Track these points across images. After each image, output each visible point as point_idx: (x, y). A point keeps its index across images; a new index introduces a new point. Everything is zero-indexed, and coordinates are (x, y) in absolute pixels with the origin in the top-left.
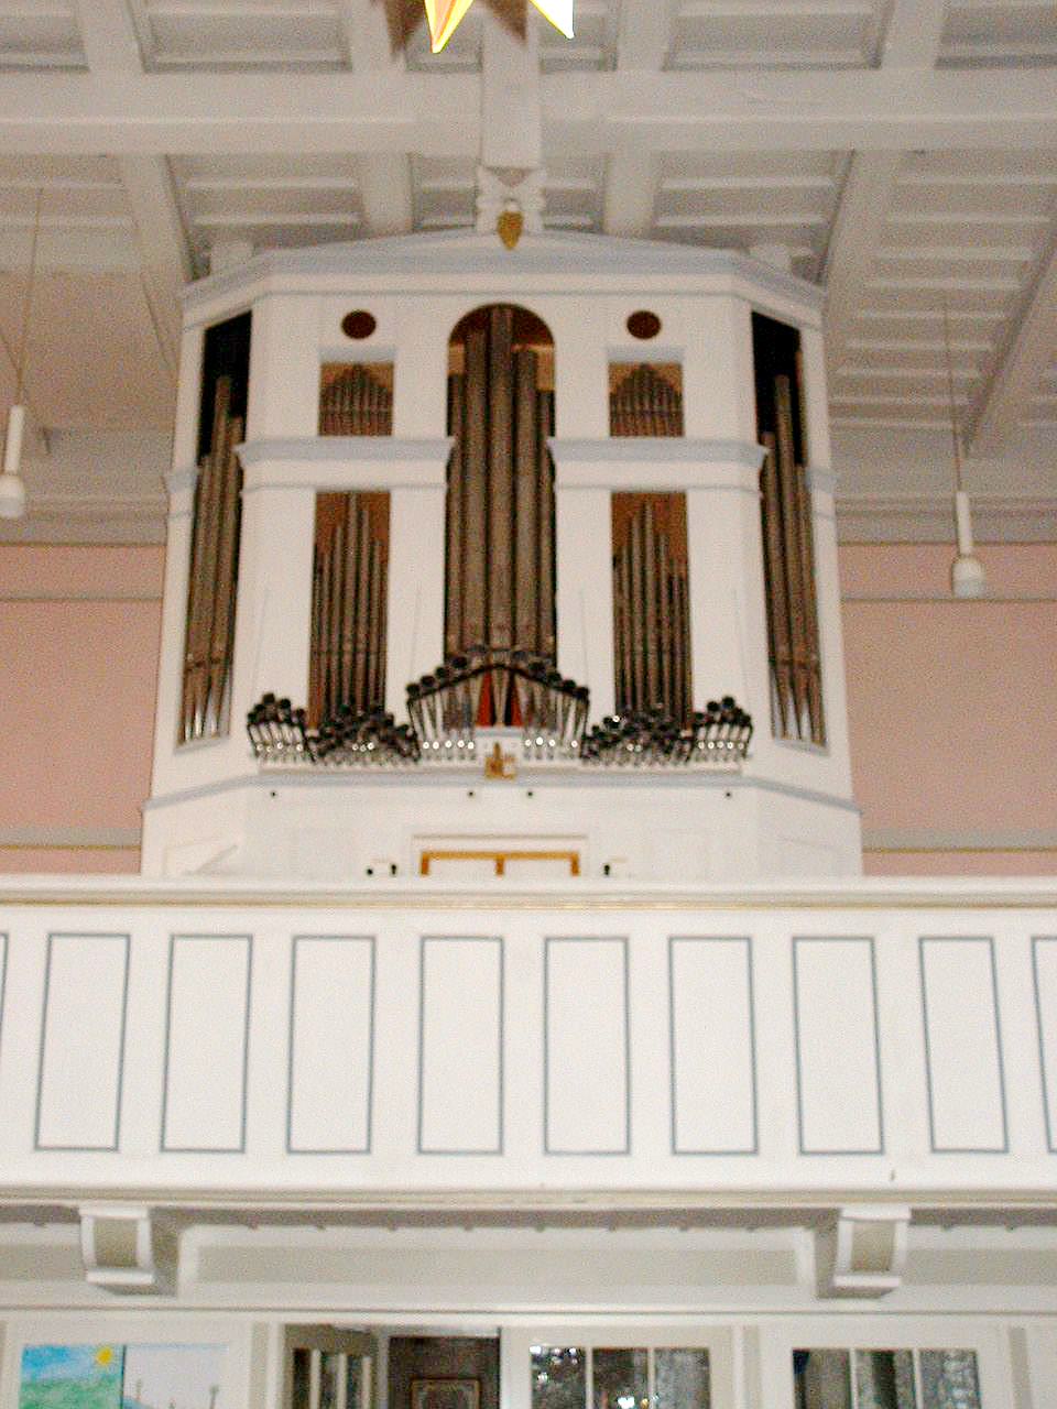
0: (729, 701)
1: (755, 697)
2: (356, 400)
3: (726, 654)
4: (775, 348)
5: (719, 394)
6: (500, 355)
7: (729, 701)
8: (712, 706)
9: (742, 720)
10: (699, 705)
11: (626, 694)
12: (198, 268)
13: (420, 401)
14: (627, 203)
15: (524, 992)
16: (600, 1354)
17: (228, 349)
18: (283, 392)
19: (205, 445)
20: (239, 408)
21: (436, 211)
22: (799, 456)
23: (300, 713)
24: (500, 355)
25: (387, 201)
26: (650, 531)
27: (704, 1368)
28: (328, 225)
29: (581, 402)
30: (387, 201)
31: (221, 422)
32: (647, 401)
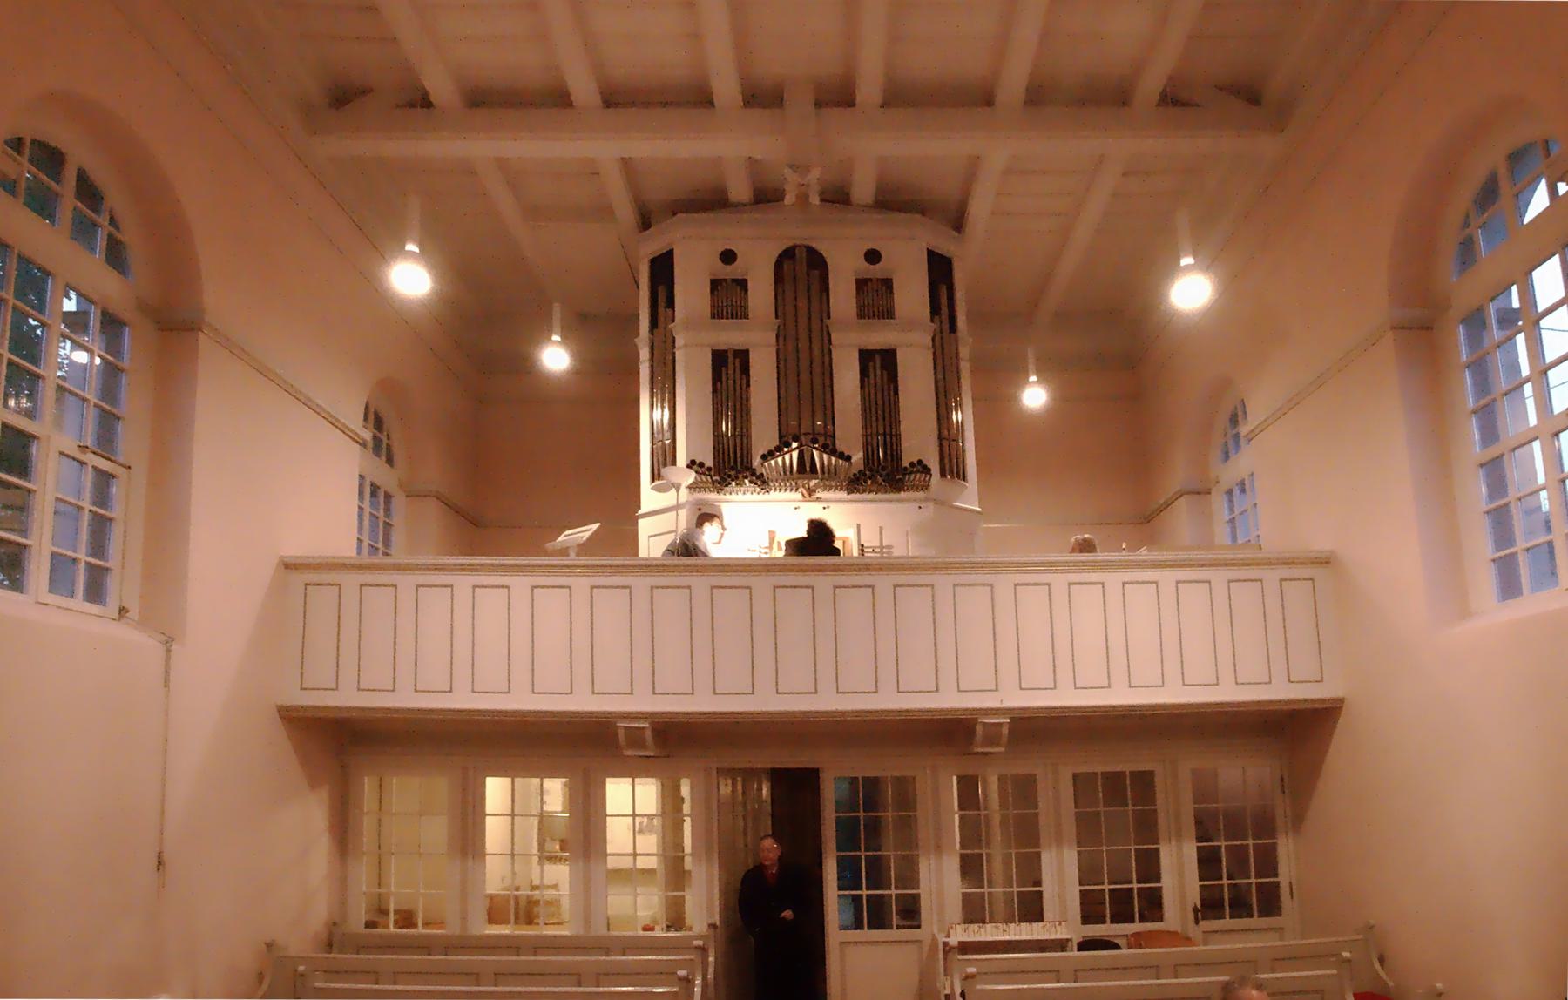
0: (920, 462)
1: (934, 464)
2: (728, 297)
3: (918, 442)
4: (940, 269)
5: (912, 295)
6: (802, 270)
7: (920, 462)
8: (912, 464)
9: (927, 470)
10: (905, 464)
11: (869, 458)
12: (645, 223)
13: (761, 295)
14: (863, 189)
15: (824, 615)
16: (915, 899)
17: (663, 268)
18: (691, 293)
19: (654, 324)
20: (671, 303)
21: (766, 197)
22: (953, 328)
23: (709, 469)
24: (802, 270)
25: (739, 190)
26: (880, 367)
27: (1000, 907)
28: (709, 201)
29: (842, 297)
30: (739, 190)
31: (661, 310)
32: (875, 297)
